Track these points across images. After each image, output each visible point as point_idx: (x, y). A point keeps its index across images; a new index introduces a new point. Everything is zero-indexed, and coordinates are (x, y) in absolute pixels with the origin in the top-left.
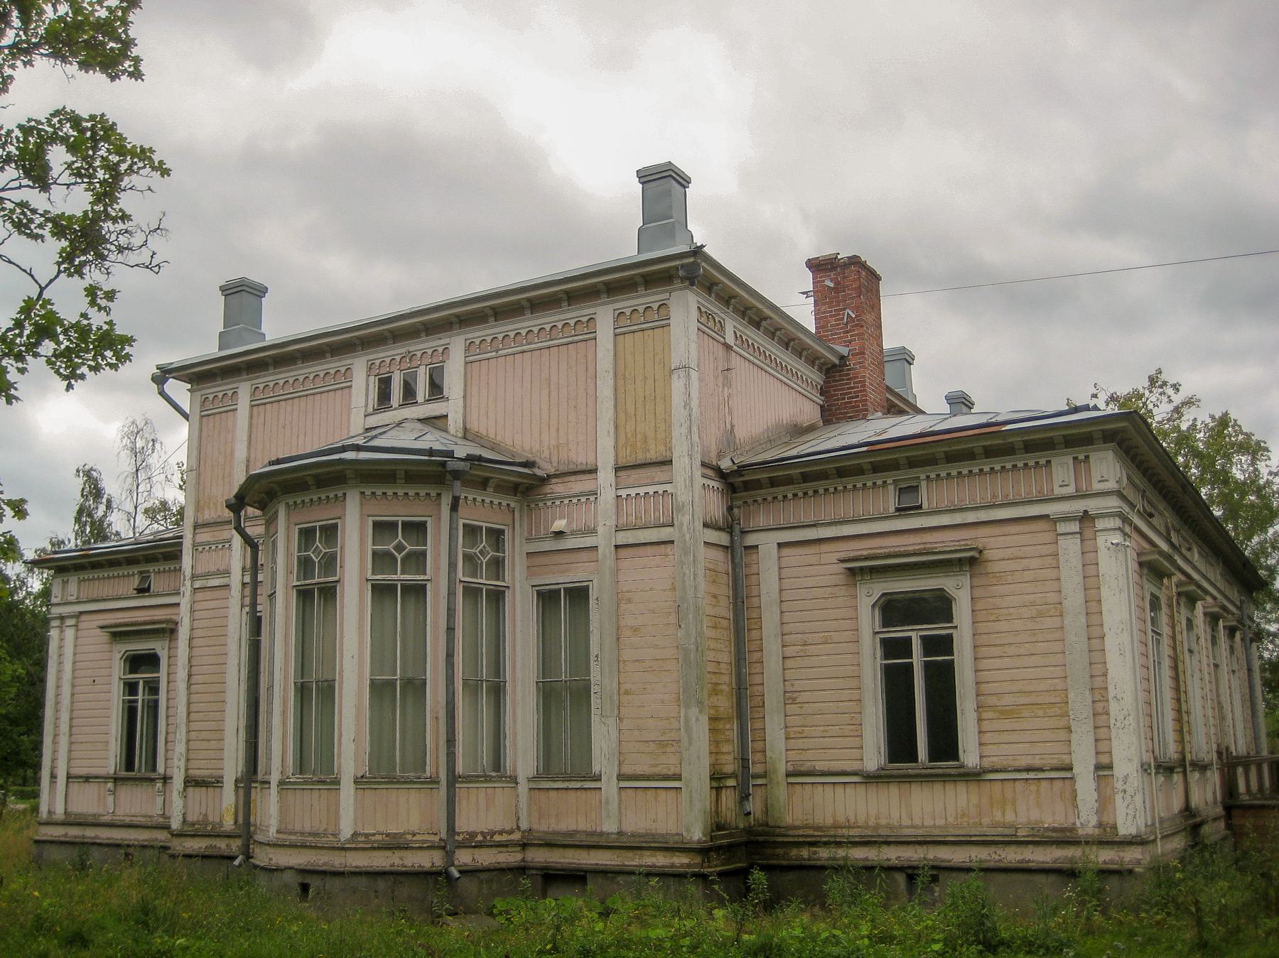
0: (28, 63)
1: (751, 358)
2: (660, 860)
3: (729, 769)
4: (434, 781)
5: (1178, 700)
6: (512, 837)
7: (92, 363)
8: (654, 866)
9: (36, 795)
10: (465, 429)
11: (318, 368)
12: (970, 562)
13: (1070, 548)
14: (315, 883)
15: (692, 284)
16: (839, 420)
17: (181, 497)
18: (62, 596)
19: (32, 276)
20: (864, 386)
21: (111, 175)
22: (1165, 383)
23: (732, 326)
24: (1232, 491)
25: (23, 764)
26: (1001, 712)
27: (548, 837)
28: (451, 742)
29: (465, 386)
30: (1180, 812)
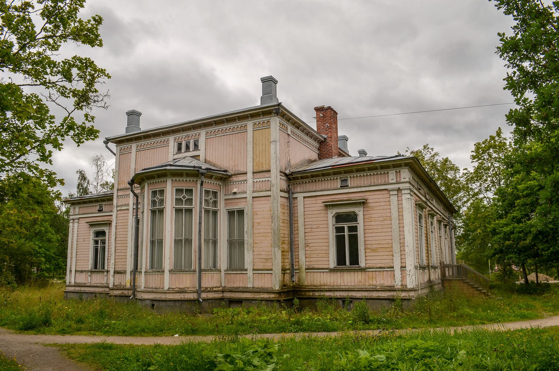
0: (66, 41)
1: (296, 138)
2: (266, 296)
3: (287, 267)
4: (195, 271)
5: (428, 247)
6: (219, 289)
7: (86, 138)
8: (264, 298)
9: (64, 278)
10: (205, 160)
11: (159, 139)
12: (363, 203)
13: (394, 199)
14: (156, 304)
15: (278, 115)
16: (324, 158)
17: (113, 181)
18: (74, 213)
19: (66, 110)
20: (332, 148)
21: (91, 77)
22: (429, 148)
23: (290, 128)
24: (448, 182)
25: (60, 268)
26: (372, 250)
27: (231, 289)
28: (200, 259)
29: (206, 146)
30: (427, 281)
